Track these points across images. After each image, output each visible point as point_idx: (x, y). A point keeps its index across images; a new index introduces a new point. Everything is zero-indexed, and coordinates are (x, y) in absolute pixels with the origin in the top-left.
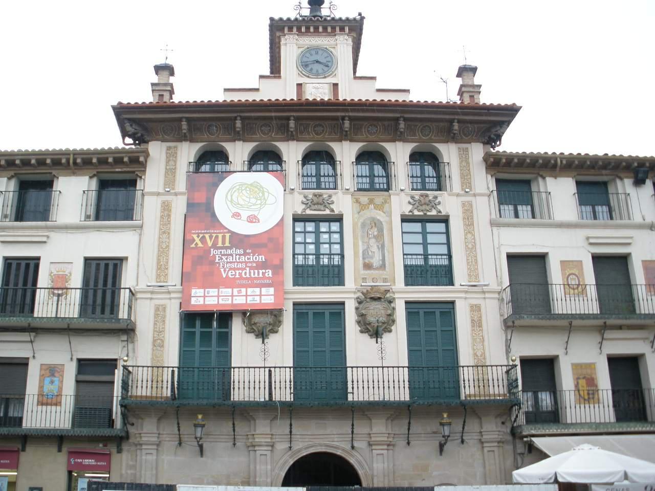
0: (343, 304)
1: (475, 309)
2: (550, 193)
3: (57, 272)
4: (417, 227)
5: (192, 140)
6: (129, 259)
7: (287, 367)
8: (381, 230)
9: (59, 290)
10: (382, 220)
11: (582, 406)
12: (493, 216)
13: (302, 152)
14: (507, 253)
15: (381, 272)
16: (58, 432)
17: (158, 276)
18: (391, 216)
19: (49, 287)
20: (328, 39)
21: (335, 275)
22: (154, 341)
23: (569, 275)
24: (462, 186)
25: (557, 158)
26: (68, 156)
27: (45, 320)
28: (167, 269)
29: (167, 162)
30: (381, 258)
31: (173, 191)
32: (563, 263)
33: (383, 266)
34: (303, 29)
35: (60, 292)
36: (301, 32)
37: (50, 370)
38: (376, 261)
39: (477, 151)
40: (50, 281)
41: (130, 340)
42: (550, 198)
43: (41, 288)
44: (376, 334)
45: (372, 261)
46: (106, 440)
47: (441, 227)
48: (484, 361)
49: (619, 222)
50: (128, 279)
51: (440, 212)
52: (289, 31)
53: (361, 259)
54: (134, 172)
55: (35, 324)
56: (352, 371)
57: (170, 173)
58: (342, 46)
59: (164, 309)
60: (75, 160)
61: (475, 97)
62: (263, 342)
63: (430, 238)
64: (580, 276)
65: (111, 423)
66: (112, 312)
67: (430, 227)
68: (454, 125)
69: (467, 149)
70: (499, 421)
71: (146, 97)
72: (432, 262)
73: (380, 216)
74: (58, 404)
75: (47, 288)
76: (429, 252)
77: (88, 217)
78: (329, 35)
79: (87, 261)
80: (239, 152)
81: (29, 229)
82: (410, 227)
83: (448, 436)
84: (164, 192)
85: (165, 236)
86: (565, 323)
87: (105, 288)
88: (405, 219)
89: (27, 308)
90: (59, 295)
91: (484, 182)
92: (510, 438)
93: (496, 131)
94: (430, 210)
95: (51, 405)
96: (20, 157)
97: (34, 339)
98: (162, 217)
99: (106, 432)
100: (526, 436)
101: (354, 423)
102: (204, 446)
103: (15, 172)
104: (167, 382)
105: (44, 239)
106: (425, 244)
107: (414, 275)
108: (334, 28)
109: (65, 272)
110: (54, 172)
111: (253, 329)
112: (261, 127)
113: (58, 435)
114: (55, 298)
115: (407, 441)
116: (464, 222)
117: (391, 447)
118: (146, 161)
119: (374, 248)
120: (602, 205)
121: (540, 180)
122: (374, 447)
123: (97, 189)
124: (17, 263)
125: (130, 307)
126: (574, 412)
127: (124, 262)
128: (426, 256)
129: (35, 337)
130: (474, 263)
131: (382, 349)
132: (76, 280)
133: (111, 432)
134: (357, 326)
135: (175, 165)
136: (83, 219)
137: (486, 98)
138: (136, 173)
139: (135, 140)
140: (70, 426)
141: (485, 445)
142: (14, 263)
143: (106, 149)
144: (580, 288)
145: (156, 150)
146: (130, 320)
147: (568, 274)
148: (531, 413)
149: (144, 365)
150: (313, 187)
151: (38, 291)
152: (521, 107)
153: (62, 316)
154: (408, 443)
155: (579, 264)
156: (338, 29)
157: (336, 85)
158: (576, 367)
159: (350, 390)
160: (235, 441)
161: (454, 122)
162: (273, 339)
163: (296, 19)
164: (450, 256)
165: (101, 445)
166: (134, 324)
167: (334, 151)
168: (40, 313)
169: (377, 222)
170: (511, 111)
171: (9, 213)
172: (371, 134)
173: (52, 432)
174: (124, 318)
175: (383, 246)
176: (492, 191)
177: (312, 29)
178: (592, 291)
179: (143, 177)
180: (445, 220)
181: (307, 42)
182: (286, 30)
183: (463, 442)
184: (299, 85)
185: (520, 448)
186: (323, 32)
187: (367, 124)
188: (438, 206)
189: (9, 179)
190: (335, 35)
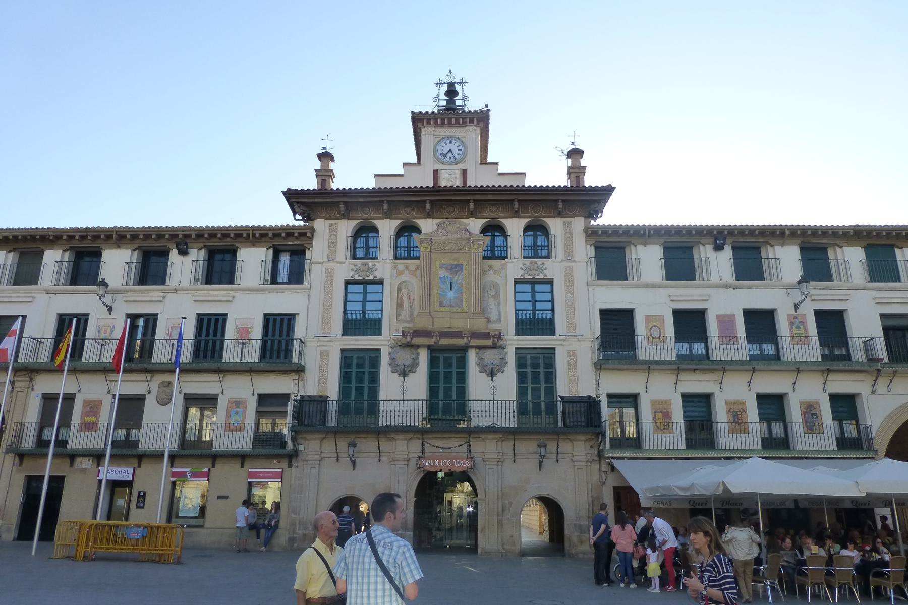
0: (379, 350)
1: (572, 354)
2: (639, 258)
3: (241, 325)
4: (528, 288)
5: (349, 218)
6: (90, 314)
7: (507, 401)
9: (243, 340)
10: (498, 282)
13: (524, 224)
14: (743, 309)
16: (241, 452)
17: (323, 328)
18: (506, 279)
19: (235, 338)
20: (459, 129)
21: (373, 327)
22: (320, 379)
23: (653, 327)
24: (565, 254)
25: (645, 229)
26: (248, 232)
27: (231, 364)
29: (330, 237)
30: (497, 313)
31: (335, 260)
32: (648, 318)
33: (499, 320)
34: (439, 121)
35: (244, 341)
36: (438, 124)
37: (236, 404)
39: (579, 224)
40: (236, 333)
41: (300, 379)
42: (708, 262)
44: (404, 373)
46: (279, 457)
47: (547, 288)
49: (706, 282)
50: (299, 331)
51: (546, 276)
52: (427, 124)
54: (303, 244)
55: (150, 367)
57: (333, 245)
58: (472, 134)
59: (328, 355)
60: (649, 232)
61: (580, 177)
62: (492, 380)
63: (538, 297)
64: (661, 328)
65: (283, 444)
66: (286, 357)
67: (538, 288)
68: (559, 204)
69: (571, 222)
70: (588, 444)
71: (312, 184)
72: (539, 316)
75: (233, 340)
76: (537, 308)
77: (266, 281)
80: (387, 228)
81: (151, 292)
82: (520, 288)
83: (544, 456)
84: (327, 260)
85: (328, 296)
86: (645, 367)
87: (273, 338)
88: (517, 282)
89: (216, 355)
90: (243, 344)
91: (584, 251)
92: (596, 458)
93: (595, 208)
94: (538, 275)
96: (233, 232)
97: (151, 379)
98: (326, 281)
99: (281, 451)
100: (608, 458)
101: (337, 443)
102: (356, 461)
103: (205, 244)
104: (422, 411)
105: (230, 299)
106: (534, 302)
107: (524, 327)
108: (464, 119)
109: (247, 325)
110: (237, 244)
111: (396, 370)
113: (241, 455)
114: (240, 346)
115: (513, 459)
116: (565, 283)
117: (500, 463)
118: (313, 236)
121: (632, 246)
122: (487, 463)
123: (207, 259)
124: (208, 318)
125: (300, 353)
127: (297, 316)
128: (534, 311)
129: (152, 377)
130: (572, 317)
132: (257, 332)
134: (477, 367)
135: (336, 239)
136: (53, 284)
137: (591, 180)
138: (305, 245)
139: (303, 217)
140: (251, 447)
141: (575, 464)
142: (206, 318)
143: (291, 225)
144: (661, 339)
145: (320, 225)
146: (301, 364)
147: (651, 326)
148: (767, 438)
149: (400, 399)
150: (530, 255)
151: (86, 341)
152: (615, 188)
153: (246, 361)
154: (514, 461)
155: (661, 318)
156: (468, 120)
157: (464, 172)
158: (654, 403)
160: (514, 457)
161: (559, 202)
162: (411, 378)
163: (433, 113)
164: (553, 311)
165: (275, 462)
166: (304, 367)
167: (549, 226)
168: (228, 359)
170: (608, 191)
171: (200, 277)
172: (492, 212)
173: (99, 452)
174: (296, 362)
175: (499, 304)
176: (590, 258)
177: (446, 121)
178: (815, 341)
179: (311, 249)
180: (550, 282)
181: (443, 132)
182: (425, 121)
183: (557, 461)
184: (436, 172)
185: (605, 468)
186: (455, 124)
188: (544, 271)
189: (199, 249)
190: (466, 126)
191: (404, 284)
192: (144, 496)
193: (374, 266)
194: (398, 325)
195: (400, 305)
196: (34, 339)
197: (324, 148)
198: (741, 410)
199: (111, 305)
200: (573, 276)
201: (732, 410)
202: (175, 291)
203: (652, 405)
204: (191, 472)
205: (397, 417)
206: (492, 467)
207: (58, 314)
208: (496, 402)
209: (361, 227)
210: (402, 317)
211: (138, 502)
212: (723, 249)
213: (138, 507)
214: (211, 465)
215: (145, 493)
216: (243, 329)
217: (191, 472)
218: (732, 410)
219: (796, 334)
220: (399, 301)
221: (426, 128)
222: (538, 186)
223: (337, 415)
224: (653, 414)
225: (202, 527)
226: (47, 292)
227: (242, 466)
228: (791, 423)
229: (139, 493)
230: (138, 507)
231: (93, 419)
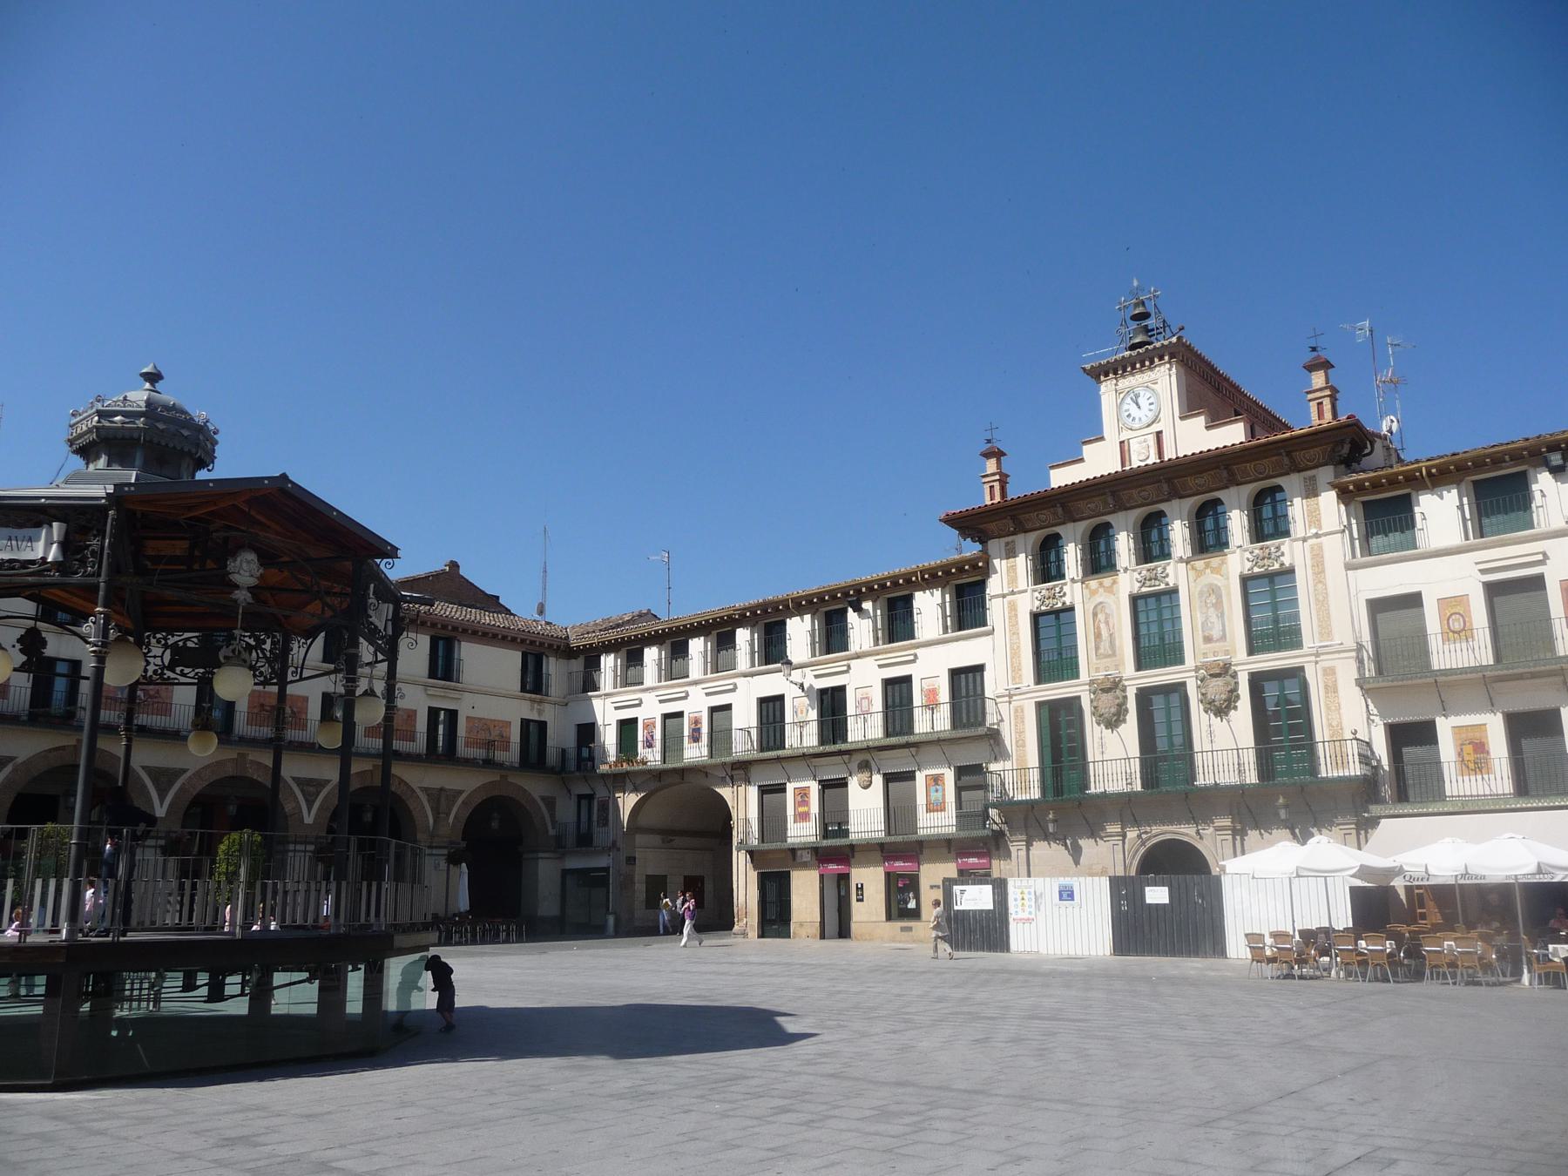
6: (987, 667)
8: (1219, 597)
10: (1219, 584)
11: (1466, 778)
12: (1349, 556)
15: (1222, 644)
23: (1451, 615)
28: (1020, 670)
30: (1221, 628)
32: (1441, 601)
33: (1223, 638)
38: (1216, 633)
45: (1211, 633)
53: (1200, 632)
64: (1465, 617)
73: (1216, 580)
74: (943, 810)
78: (1150, 369)
81: (835, 661)
95: (937, 811)
119: (1214, 619)
120: (47, 986)
126: (1456, 784)
130: (1326, 619)
132: (944, 695)
136: (872, 645)
144: (1465, 633)
147: (1449, 614)
169: (1214, 587)
175: (1222, 614)
191: (1100, 607)
193: (1278, 548)
194: (1099, 661)
195: (1098, 636)
196: (742, 729)
197: (989, 441)
199: (801, 682)
200: (1322, 557)
202: (858, 656)
203: (1454, 734)
205: (1115, 781)
206: (1116, 842)
207: (882, 680)
208: (1023, 771)
210: (1101, 651)
211: (857, 895)
212: (1564, 471)
213: (858, 900)
215: (862, 885)
221: (1104, 384)
224: (1459, 748)
226: (745, 675)
228: (1437, 763)
229: (857, 885)
230: (858, 900)
231: (806, 809)
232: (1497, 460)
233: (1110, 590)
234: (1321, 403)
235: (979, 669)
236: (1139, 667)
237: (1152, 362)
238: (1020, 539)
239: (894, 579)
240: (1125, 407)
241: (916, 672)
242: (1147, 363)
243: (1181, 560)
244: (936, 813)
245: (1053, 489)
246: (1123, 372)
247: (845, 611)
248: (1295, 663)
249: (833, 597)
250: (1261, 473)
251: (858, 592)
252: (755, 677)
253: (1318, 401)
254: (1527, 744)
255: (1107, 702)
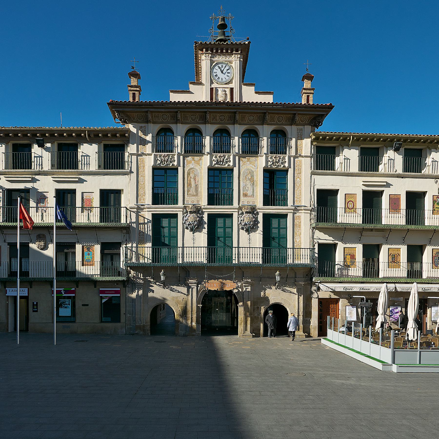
23: (349, 201)
33: (253, 196)
38: (250, 193)
43: (32, 207)
48: (300, 245)
56: (235, 249)
79: (57, 190)
112: (191, 116)
131: (250, 239)
132: (96, 202)
133: (102, 279)
144: (354, 209)
147: (348, 201)
159: (234, 258)
178: (360, 211)
187: (248, 116)
192: (37, 305)
198: (397, 254)
201: (392, 254)
204: (64, 290)
209: (274, 130)
211: (33, 308)
214: (76, 286)
215: (37, 303)
216: (87, 200)
217: (64, 290)
218: (392, 254)
219: (436, 208)
220: (188, 182)
222: (189, 102)
223: (288, 256)
225: (74, 322)
227: (95, 287)
230: (34, 311)
232: (372, 139)
233: (198, 163)
234: (309, 96)
235: (118, 193)
236: (265, 204)
237: (232, 52)
238: (151, 126)
239: (70, 133)
240: (215, 71)
241: (79, 188)
242: (229, 51)
243: (208, 153)
244: (89, 266)
245: (171, 102)
246: (226, 52)
247: (29, 147)
248: (271, 212)
249: (25, 135)
250: (279, 121)
251: (43, 135)
252: (406, 178)
253: (307, 95)
254: (17, 242)
255: (247, 218)
